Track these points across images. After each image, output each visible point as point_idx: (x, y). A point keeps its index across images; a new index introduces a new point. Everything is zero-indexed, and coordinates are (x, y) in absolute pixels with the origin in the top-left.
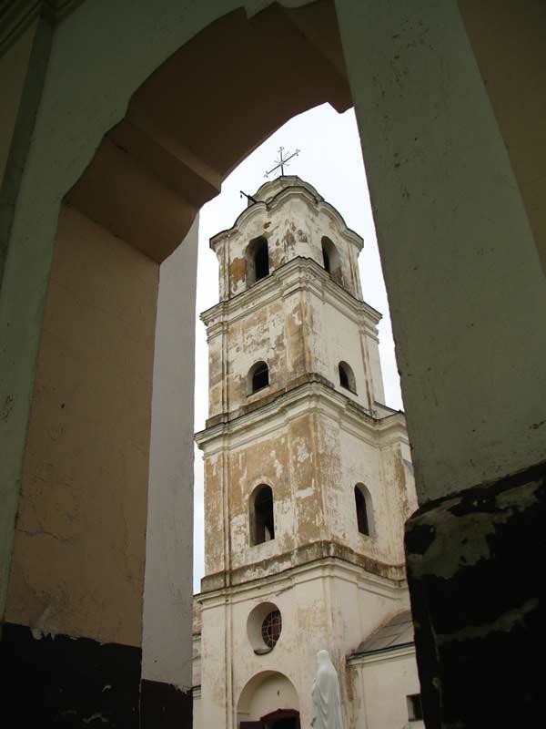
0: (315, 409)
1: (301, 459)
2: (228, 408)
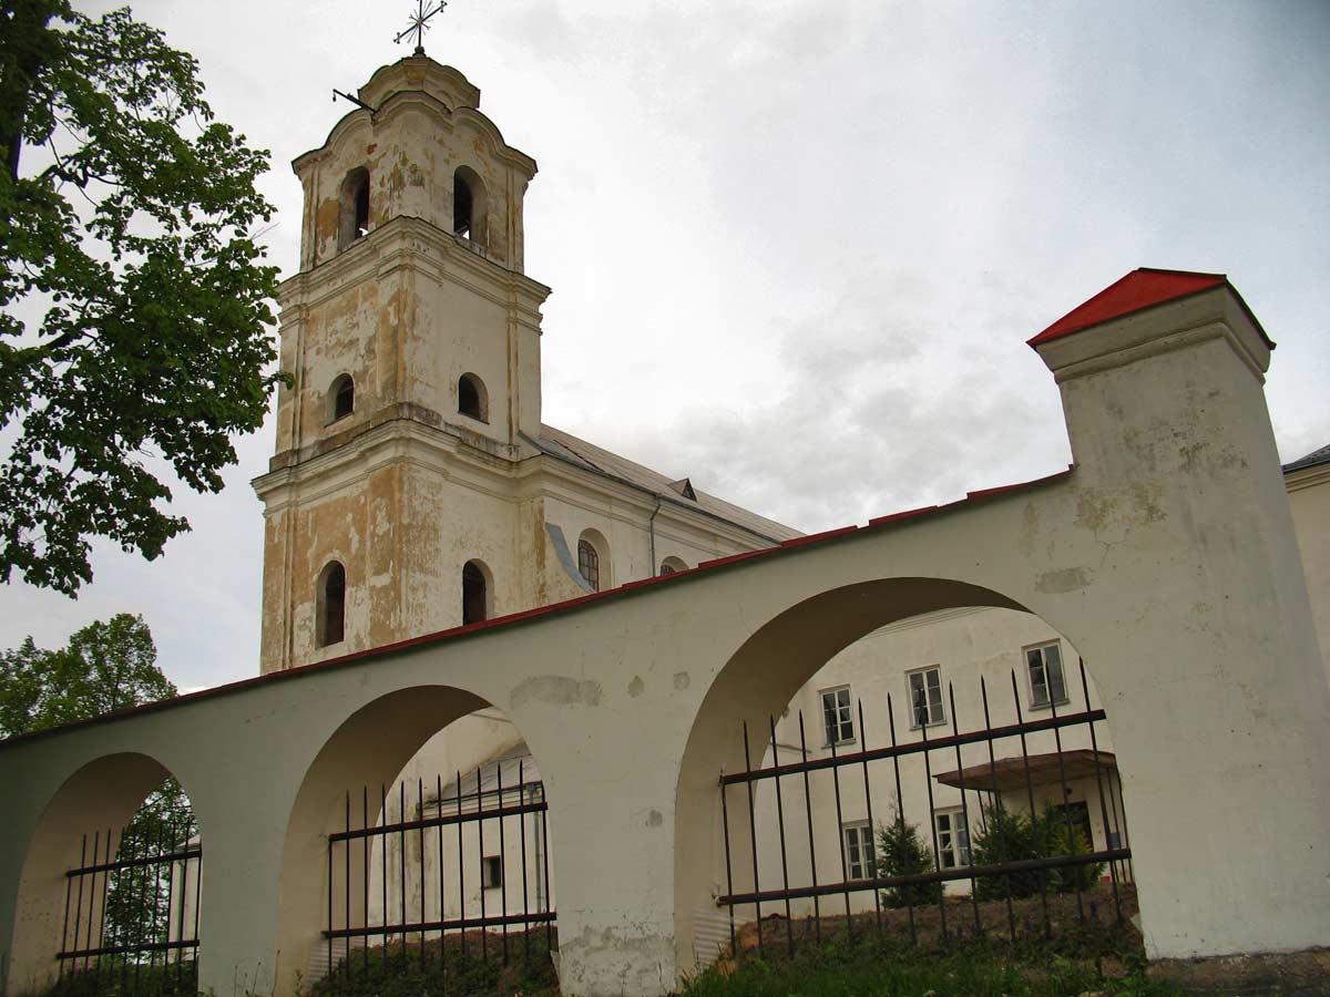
1: (380, 531)
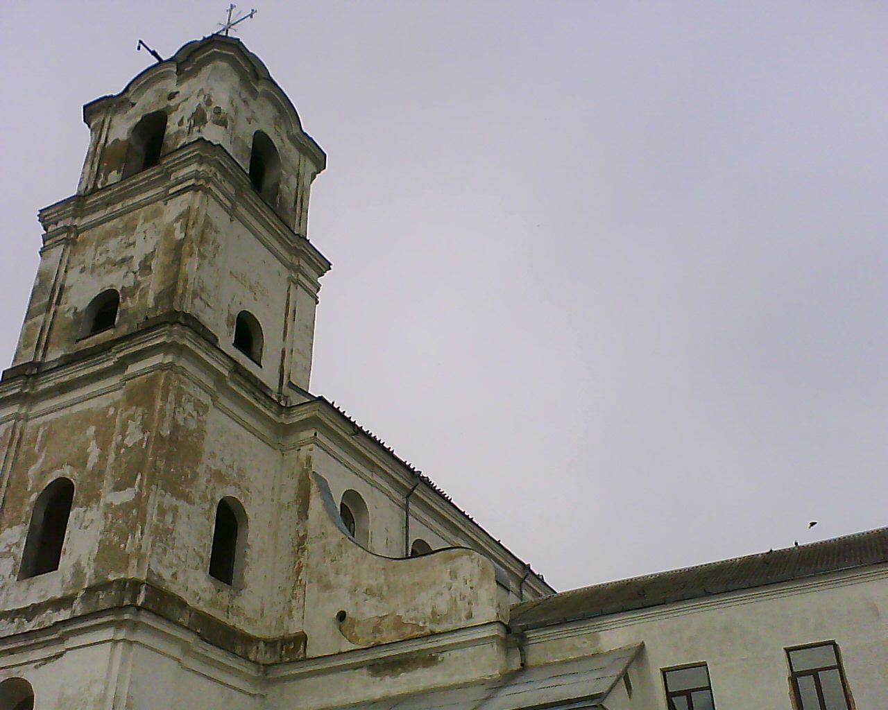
0: (171, 366)
1: (129, 442)
2: (44, 356)
